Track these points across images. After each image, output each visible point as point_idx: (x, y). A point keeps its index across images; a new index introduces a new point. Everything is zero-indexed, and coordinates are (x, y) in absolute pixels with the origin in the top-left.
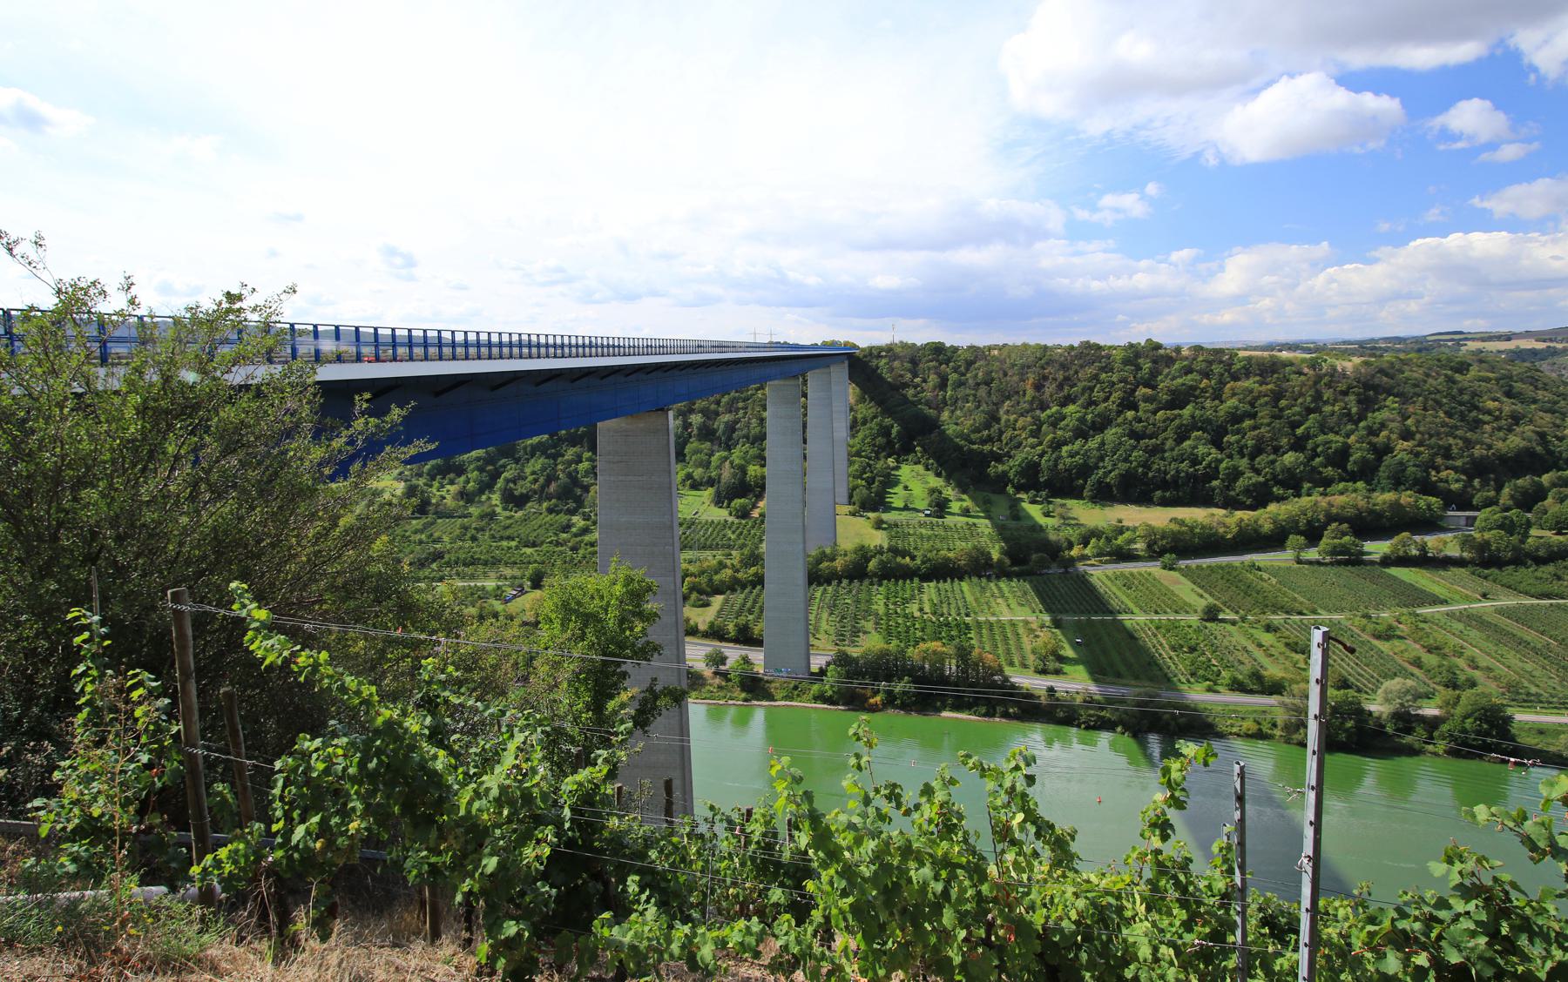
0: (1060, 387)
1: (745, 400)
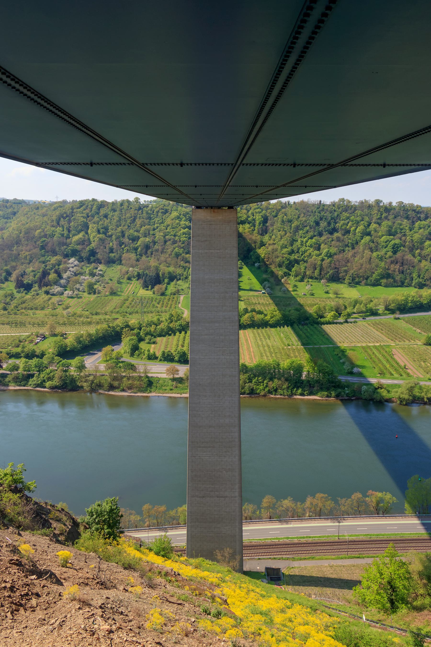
0: (329, 224)
1: (154, 230)
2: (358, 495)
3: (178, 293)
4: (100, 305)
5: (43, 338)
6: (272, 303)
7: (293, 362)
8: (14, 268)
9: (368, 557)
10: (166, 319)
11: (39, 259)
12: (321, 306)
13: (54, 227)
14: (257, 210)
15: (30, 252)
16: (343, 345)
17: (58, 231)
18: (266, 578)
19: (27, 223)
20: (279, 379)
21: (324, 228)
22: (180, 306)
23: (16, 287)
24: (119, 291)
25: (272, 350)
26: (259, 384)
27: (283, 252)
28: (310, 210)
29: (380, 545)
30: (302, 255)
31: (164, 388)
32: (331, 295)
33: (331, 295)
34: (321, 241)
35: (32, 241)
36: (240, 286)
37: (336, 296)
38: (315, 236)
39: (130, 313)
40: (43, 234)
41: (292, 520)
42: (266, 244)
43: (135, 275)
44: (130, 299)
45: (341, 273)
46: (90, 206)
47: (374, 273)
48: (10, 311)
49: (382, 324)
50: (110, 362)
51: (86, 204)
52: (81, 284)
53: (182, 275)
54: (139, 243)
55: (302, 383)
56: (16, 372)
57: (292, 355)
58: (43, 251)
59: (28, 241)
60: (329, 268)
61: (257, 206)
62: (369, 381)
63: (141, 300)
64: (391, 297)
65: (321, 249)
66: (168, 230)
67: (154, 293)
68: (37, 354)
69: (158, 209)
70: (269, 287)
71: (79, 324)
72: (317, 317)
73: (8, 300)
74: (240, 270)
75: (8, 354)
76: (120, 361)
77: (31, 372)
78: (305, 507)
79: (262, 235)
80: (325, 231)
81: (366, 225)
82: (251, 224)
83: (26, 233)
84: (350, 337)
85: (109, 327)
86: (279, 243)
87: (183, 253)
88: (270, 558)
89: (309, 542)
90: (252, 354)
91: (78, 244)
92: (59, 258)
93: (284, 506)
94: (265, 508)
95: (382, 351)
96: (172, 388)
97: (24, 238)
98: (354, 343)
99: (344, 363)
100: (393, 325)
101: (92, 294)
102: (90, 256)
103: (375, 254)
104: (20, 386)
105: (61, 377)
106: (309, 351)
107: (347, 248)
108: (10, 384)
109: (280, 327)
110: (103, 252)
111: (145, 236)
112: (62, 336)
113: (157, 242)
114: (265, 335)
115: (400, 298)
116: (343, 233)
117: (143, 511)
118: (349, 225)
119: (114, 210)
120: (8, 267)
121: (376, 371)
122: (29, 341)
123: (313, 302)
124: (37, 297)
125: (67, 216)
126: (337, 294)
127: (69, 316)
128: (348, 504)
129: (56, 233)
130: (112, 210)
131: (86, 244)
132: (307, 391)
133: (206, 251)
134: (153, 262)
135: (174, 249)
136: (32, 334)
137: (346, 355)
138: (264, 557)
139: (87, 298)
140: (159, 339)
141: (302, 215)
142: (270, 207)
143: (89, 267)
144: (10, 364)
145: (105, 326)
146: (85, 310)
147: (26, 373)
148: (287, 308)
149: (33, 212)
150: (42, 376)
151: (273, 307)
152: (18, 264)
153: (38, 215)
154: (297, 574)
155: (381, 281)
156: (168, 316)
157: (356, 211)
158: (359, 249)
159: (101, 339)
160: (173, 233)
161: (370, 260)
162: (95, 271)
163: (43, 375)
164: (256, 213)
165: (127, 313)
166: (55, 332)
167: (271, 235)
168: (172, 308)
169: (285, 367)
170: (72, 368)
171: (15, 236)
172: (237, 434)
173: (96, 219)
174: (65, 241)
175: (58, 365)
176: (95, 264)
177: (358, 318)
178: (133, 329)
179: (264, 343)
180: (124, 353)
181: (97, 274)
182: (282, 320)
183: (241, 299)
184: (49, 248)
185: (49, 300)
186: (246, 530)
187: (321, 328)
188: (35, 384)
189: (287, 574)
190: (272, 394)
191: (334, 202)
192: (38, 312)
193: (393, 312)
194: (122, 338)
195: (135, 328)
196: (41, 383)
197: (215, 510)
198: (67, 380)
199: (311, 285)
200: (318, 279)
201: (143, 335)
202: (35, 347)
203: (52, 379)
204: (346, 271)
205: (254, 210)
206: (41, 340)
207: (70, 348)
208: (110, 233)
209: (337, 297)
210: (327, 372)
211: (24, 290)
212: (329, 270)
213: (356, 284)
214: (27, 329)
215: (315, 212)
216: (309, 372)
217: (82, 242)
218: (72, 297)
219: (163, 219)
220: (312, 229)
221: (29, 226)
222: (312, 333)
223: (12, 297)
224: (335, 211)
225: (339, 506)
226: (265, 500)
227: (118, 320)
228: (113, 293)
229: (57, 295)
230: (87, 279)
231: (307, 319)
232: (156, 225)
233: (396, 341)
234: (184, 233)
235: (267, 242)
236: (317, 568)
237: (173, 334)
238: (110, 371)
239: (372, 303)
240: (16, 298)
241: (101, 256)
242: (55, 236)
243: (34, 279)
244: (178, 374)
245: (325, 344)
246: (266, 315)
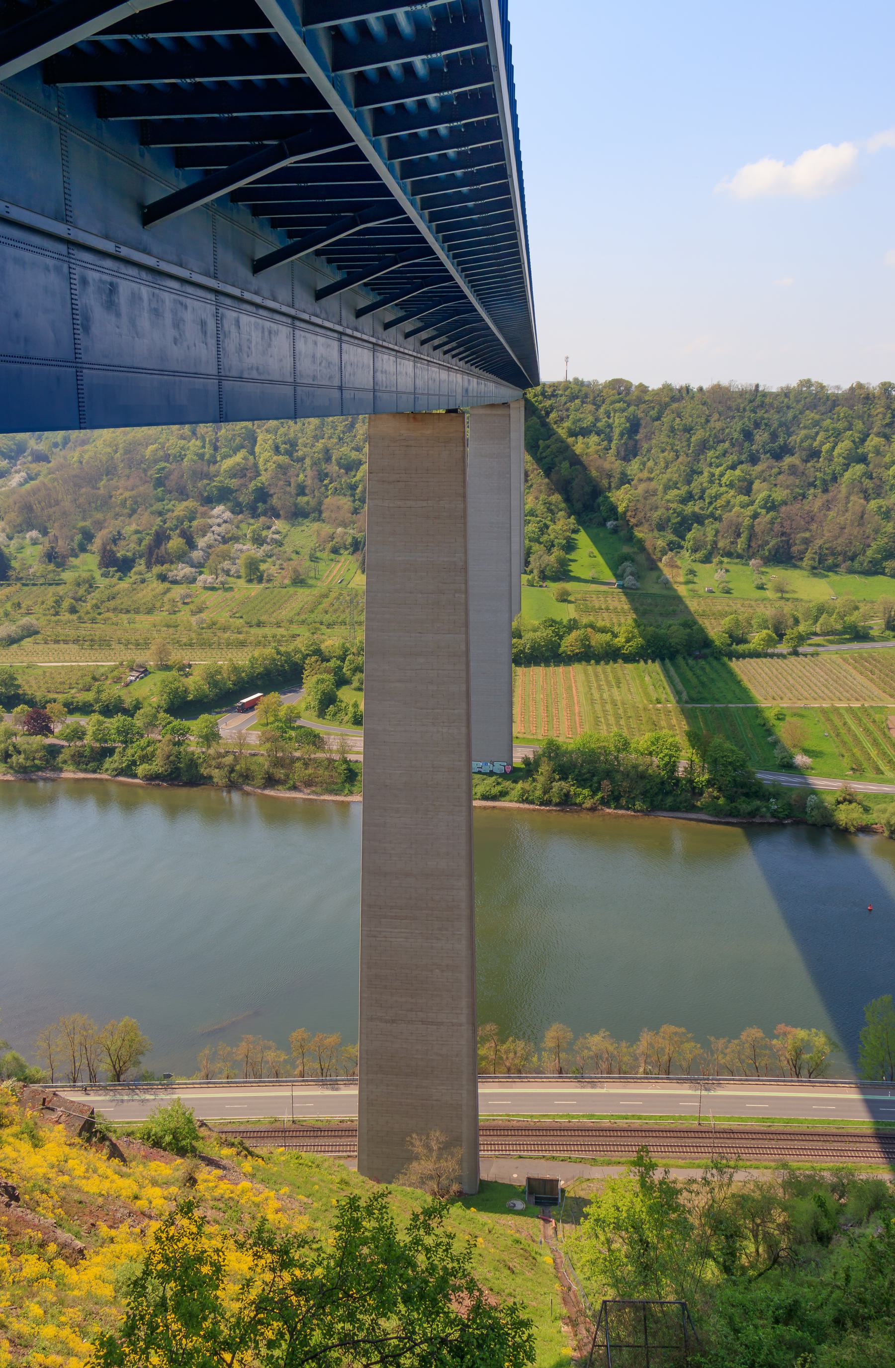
0: (774, 436)
2: (754, 1033)
4: (268, 606)
5: (143, 672)
8: (100, 525)
12: (740, 618)
13: (184, 439)
14: (617, 405)
18: (523, 1199)
21: (763, 446)
24: (311, 578)
25: (621, 711)
27: (668, 497)
28: (734, 405)
29: (789, 1142)
30: (710, 503)
32: (770, 594)
33: (770, 594)
34: (754, 474)
36: (571, 571)
37: (779, 595)
38: (742, 463)
39: (329, 625)
40: (161, 453)
42: (632, 480)
43: (347, 543)
44: (333, 595)
47: (869, 546)
48: (83, 615)
52: (233, 560)
56: (79, 743)
57: (663, 723)
58: (159, 490)
59: (130, 468)
61: (617, 397)
62: (809, 784)
65: (754, 491)
68: (126, 706)
70: (632, 574)
72: (729, 642)
73: (81, 591)
74: (573, 536)
75: (66, 705)
77: (109, 745)
79: (626, 459)
80: (766, 453)
81: (857, 440)
82: (602, 436)
83: (127, 451)
84: (797, 685)
85: (278, 653)
86: (660, 477)
88: (544, 1157)
89: (633, 1127)
90: (577, 718)
91: (234, 476)
92: (192, 504)
93: (593, 1048)
101: (255, 582)
102: (257, 500)
103: (873, 505)
104: (85, 771)
105: (168, 757)
107: (812, 491)
108: (65, 767)
109: (646, 662)
116: (805, 458)
118: (818, 438)
120: (87, 523)
121: (846, 762)
122: (113, 678)
123: (727, 608)
124: (143, 586)
126: (782, 591)
127: (203, 628)
129: (188, 452)
131: (249, 475)
136: (121, 664)
139: (244, 589)
141: (716, 416)
142: (647, 398)
144: (68, 726)
145: (269, 651)
146: (237, 615)
150: (130, 752)
157: (837, 409)
158: (840, 492)
161: (862, 517)
162: (264, 533)
164: (615, 411)
166: (169, 660)
167: (645, 459)
170: (192, 738)
171: (104, 459)
172: (463, 894)
174: (205, 469)
175: (163, 731)
177: (823, 646)
179: (606, 696)
180: (307, 709)
181: (268, 540)
183: (569, 598)
184: (171, 483)
185: (165, 593)
186: (484, 1094)
190: (609, 807)
191: (788, 387)
194: (304, 676)
196: (128, 766)
199: (727, 571)
200: (743, 557)
202: (123, 693)
204: (807, 542)
205: (611, 404)
206: (138, 677)
208: (300, 453)
209: (782, 598)
210: (730, 763)
211: (117, 571)
212: (768, 538)
213: (828, 571)
214: (112, 653)
215: (744, 410)
217: (240, 473)
218: (213, 589)
220: (736, 448)
221: (134, 437)
223: (91, 586)
224: (788, 407)
225: (712, 1055)
228: (299, 581)
230: (247, 549)
238: (268, 745)
239: (856, 613)
240: (98, 587)
243: (138, 548)
246: (615, 636)
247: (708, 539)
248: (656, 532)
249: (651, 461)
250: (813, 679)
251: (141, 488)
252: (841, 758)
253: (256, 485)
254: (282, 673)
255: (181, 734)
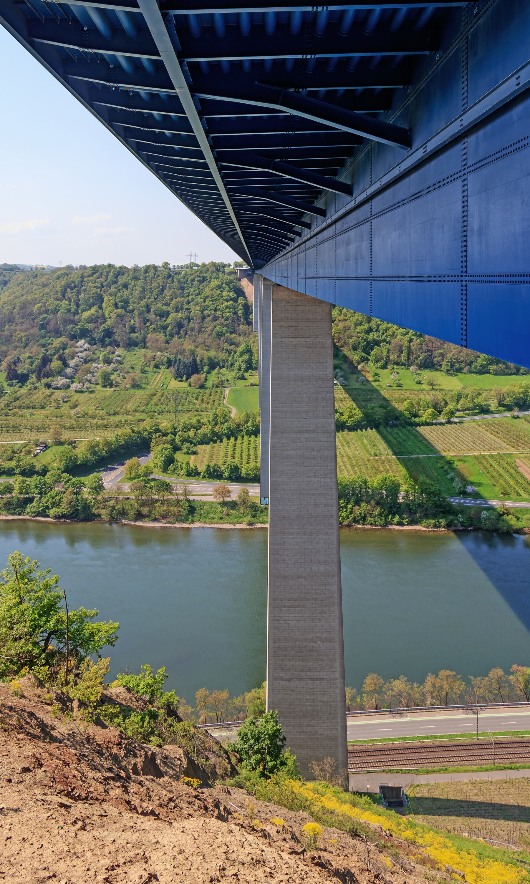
1: (188, 303)
3: (222, 385)
4: (118, 403)
5: (45, 447)
6: (348, 398)
7: (386, 478)
9: (524, 768)
10: (209, 421)
11: (38, 341)
12: (414, 402)
13: (58, 300)
15: (27, 333)
16: (449, 455)
17: (63, 306)
19: (22, 295)
20: (368, 502)
22: (225, 402)
23: (6, 378)
24: (143, 383)
25: (354, 462)
26: (341, 509)
27: (357, 330)
30: (383, 334)
31: (210, 516)
32: (425, 387)
33: (425, 387)
35: (28, 318)
37: (431, 387)
40: (43, 309)
41: (407, 710)
42: (335, 321)
43: (164, 361)
44: (159, 394)
45: (436, 357)
46: (105, 274)
47: (479, 357)
49: (497, 425)
50: (136, 480)
51: (100, 271)
52: (92, 373)
53: (227, 362)
54: (169, 320)
55: (400, 508)
56: (9, 495)
57: (381, 469)
59: (23, 318)
60: (419, 350)
63: (175, 393)
64: (506, 389)
66: (206, 303)
67: (190, 386)
69: (193, 276)
70: (342, 376)
71: (92, 427)
72: (410, 417)
76: (150, 478)
77: (30, 495)
78: (425, 690)
83: (21, 308)
85: (133, 432)
86: (351, 319)
87: (227, 332)
88: (384, 770)
92: (64, 339)
93: (395, 689)
94: (368, 692)
95: (502, 462)
96: (221, 515)
97: (18, 314)
98: (463, 452)
99: (452, 479)
100: (512, 426)
101: (108, 386)
104: (14, 514)
105: (71, 502)
106: (404, 462)
109: (361, 430)
110: (122, 331)
111: (177, 311)
112: (70, 444)
113: (193, 319)
114: (343, 441)
115: (518, 390)
117: (196, 699)
119: (137, 279)
122: (26, 451)
123: (402, 396)
124: (35, 391)
125: (75, 287)
126: (432, 385)
128: (485, 686)
129: (61, 308)
130: (134, 278)
131: (100, 321)
132: (406, 518)
133: (291, 339)
134: (188, 345)
135: (215, 327)
136: (30, 442)
137: (455, 469)
138: (375, 769)
140: (200, 448)
143: (103, 351)
145: (127, 430)
146: (99, 408)
147: (22, 496)
148: (369, 405)
149: (30, 281)
150: (44, 500)
151: (350, 403)
152: (10, 347)
153: (37, 285)
154: (426, 795)
155: (489, 368)
156: (211, 417)
159: (123, 448)
160: (213, 307)
162: (111, 356)
163: (46, 500)
165: (155, 412)
168: (216, 405)
169: (375, 485)
170: (85, 489)
171: (7, 312)
172: (335, 588)
173: (113, 289)
174: (72, 318)
175: (66, 486)
176: (111, 348)
177: (464, 417)
178: (165, 435)
180: (155, 467)
181: (114, 361)
182: (364, 421)
184: (51, 327)
187: (417, 431)
188: (35, 512)
189: (411, 796)
190: (359, 524)
192: (35, 412)
193: (509, 408)
194: (151, 446)
195: (168, 433)
196: (44, 510)
197: (307, 699)
198: (78, 506)
200: (407, 365)
201: (179, 443)
202: (34, 460)
203: (59, 505)
204: (442, 355)
206: (41, 450)
207: (82, 461)
208: (131, 308)
209: (433, 389)
210: (432, 492)
211: (18, 382)
212: (419, 353)
216: (407, 492)
218: (81, 392)
219: (199, 289)
222: (405, 438)
225: (472, 689)
226: (368, 681)
227: (145, 423)
228: (136, 386)
229: (61, 389)
230: (101, 367)
231: (397, 418)
232: (190, 297)
233: (519, 448)
234: (227, 307)
235: (336, 318)
236: (453, 786)
237: (218, 441)
239: (480, 397)
240: (7, 393)
241: (119, 338)
242: (60, 312)
243: (31, 367)
244: (229, 496)
245: (424, 453)
246: (342, 414)
247: (384, 355)
248: (352, 351)
249: (345, 309)
250: (464, 438)
251: (32, 331)
252: (493, 487)
253: (104, 327)
254: (136, 445)
255: (78, 487)
